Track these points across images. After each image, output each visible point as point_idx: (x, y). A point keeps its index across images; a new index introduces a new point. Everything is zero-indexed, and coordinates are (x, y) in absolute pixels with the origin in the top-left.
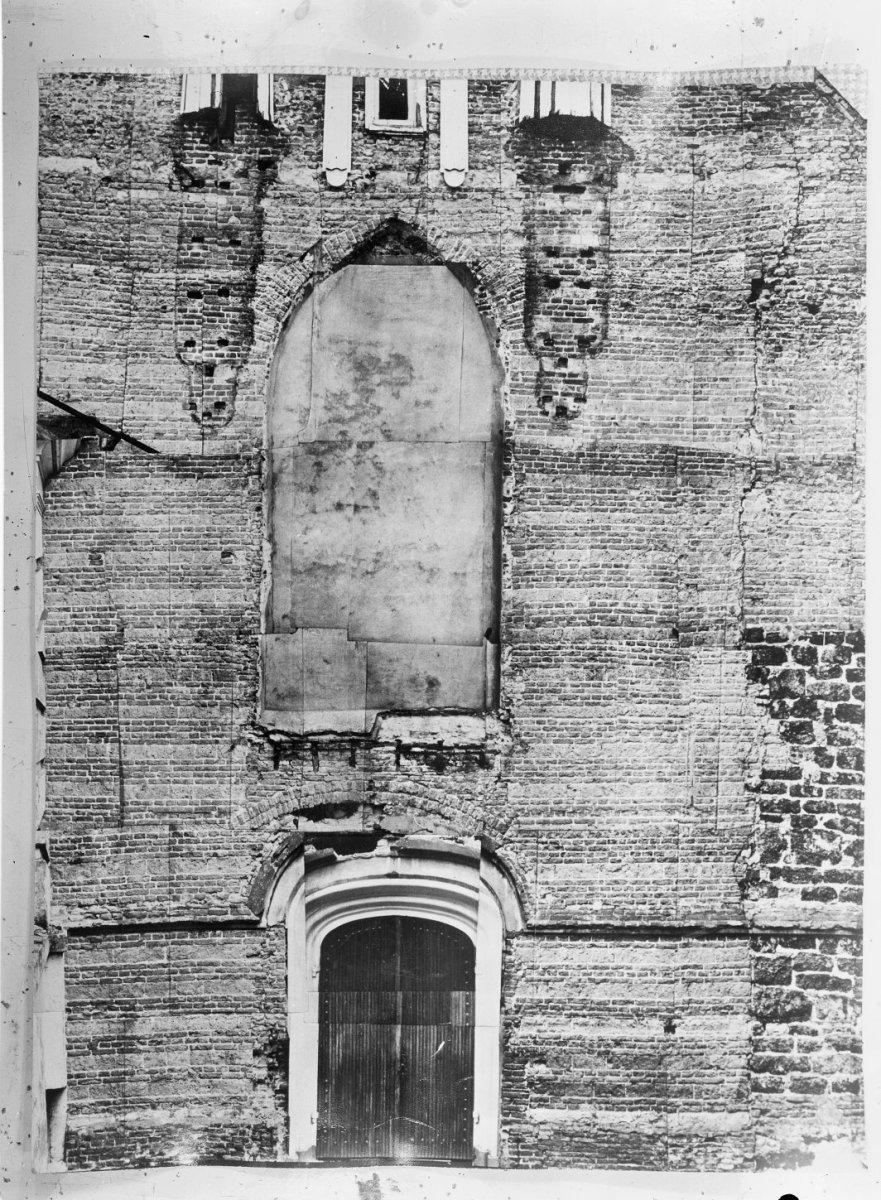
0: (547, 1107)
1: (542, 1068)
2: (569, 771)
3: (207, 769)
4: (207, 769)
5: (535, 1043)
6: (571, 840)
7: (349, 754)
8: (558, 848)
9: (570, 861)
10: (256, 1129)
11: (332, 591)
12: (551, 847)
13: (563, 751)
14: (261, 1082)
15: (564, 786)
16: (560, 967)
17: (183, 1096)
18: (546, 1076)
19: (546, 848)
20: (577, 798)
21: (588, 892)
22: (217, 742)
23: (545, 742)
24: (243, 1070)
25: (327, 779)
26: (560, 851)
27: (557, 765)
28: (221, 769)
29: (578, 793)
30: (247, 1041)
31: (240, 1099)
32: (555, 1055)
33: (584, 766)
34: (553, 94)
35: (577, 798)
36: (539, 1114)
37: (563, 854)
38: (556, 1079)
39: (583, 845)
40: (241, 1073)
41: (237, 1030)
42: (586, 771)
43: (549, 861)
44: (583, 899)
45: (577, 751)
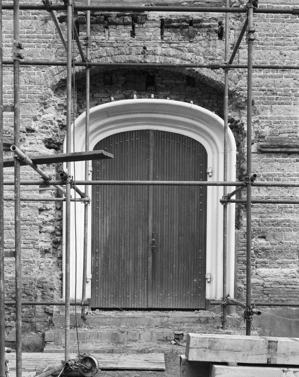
0: (266, 267)
1: (262, 241)
2: (282, 42)
3: (28, 37)
4: (28, 37)
5: (259, 225)
6: (282, 89)
7: (130, 28)
8: (273, 94)
9: (282, 104)
10: (39, 282)
11: (51, 246)
12: (269, 93)
13: (278, 28)
14: (46, 251)
15: (278, 53)
16: (275, 175)
17: (33, 95)
18: (266, 247)
19: (266, 94)
20: (286, 60)
21: (294, 125)
22: (35, 18)
23: (265, 21)
24: (32, 243)
25: (115, 45)
26: (275, 97)
27: (273, 38)
28: (38, 37)
29: (287, 57)
30: (35, 224)
31: (31, 262)
32: (272, 233)
33: (292, 38)
34: (224, 237)
35: (286, 60)
36: (263, 271)
37: (277, 99)
38: (273, 248)
39: (290, 92)
40: (31, 245)
41: (28, 217)
42: (293, 42)
43: (267, 103)
44: (291, 129)
45: (287, 27)
